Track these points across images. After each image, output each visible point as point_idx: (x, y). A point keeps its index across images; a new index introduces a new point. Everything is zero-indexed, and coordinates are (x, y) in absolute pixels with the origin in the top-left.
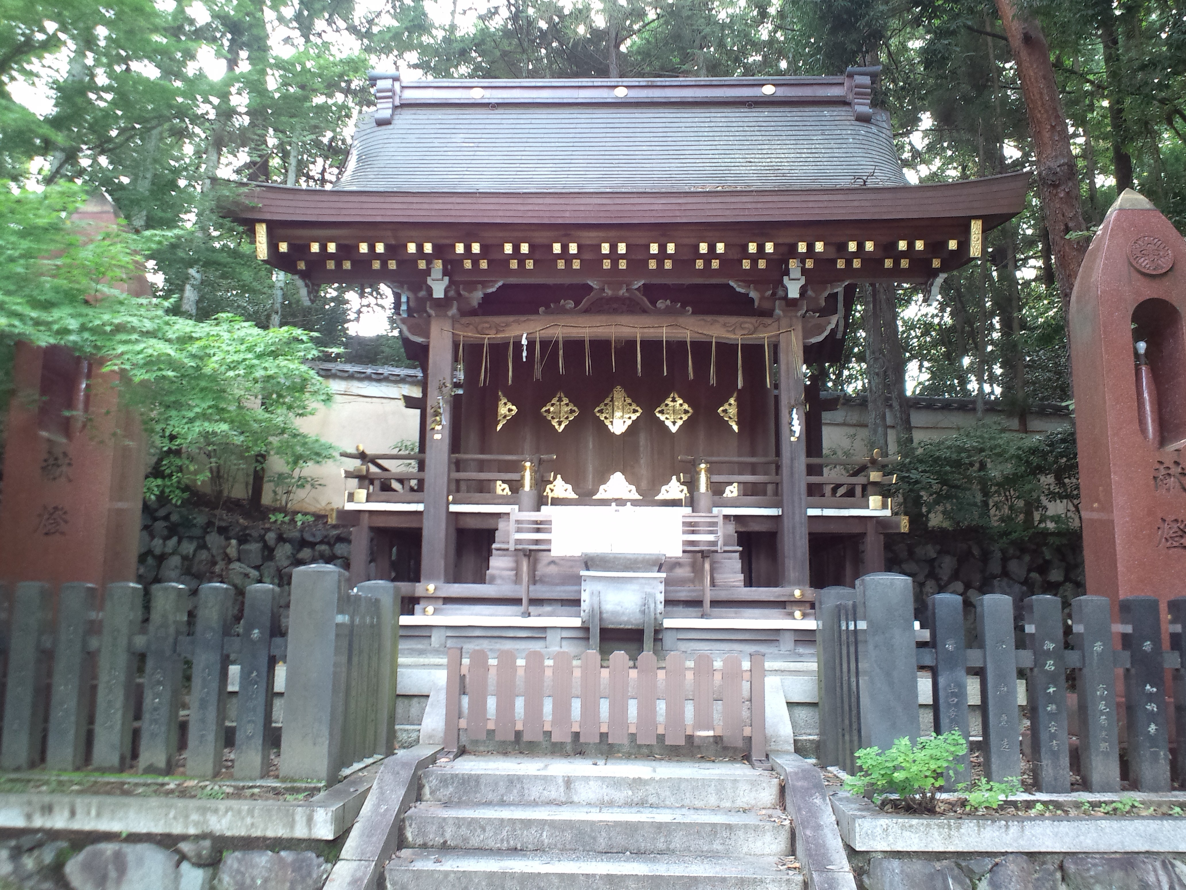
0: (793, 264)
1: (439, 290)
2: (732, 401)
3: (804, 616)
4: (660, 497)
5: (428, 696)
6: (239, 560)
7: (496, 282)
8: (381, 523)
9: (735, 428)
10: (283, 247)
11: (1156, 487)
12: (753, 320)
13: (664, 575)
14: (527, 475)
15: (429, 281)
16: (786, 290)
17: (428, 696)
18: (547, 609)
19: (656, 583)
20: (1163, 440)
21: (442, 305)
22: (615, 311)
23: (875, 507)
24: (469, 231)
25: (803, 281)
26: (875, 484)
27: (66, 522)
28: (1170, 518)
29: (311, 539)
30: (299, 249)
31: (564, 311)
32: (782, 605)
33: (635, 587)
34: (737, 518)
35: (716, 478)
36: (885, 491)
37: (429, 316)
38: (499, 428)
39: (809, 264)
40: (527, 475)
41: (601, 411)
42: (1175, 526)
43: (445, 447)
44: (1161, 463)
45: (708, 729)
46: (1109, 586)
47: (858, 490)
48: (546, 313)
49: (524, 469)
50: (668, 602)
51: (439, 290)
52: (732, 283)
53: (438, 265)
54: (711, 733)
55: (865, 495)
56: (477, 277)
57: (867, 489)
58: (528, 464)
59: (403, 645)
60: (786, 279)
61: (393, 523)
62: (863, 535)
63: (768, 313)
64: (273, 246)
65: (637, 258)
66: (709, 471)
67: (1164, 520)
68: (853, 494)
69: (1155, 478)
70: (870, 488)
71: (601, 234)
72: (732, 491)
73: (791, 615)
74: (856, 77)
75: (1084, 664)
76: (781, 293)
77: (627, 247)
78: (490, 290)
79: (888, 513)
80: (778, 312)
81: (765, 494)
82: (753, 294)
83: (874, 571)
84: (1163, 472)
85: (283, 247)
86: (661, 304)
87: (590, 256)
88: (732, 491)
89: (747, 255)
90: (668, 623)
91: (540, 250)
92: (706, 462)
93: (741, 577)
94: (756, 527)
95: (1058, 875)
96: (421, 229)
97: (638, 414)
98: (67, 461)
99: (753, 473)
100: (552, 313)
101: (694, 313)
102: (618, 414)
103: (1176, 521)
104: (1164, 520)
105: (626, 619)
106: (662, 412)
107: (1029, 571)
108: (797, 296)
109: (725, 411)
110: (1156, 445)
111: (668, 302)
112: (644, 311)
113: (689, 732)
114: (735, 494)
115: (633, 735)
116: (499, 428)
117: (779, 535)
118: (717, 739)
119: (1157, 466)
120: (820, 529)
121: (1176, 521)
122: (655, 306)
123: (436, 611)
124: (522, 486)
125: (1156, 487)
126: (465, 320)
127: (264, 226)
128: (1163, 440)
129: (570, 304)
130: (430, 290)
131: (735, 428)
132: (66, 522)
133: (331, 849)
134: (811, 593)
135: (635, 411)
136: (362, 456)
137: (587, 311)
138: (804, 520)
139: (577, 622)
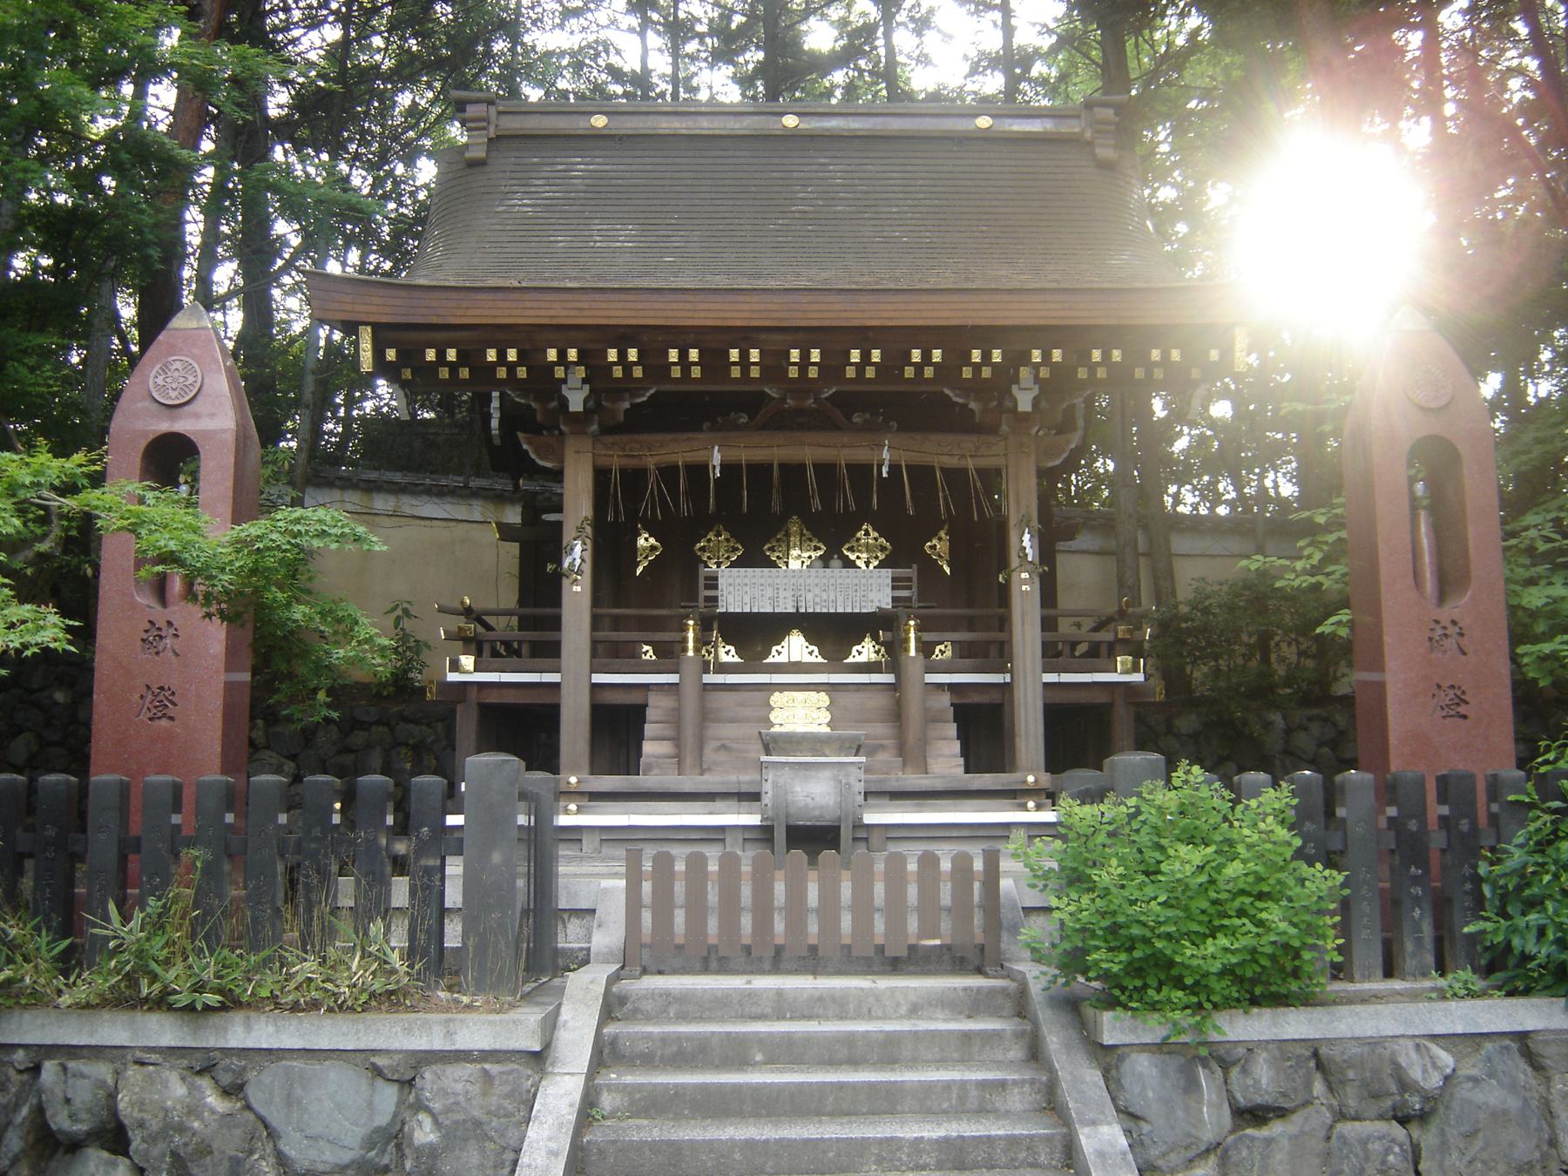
0: (1025, 373)
1: (576, 400)
2: (942, 534)
3: (1039, 807)
4: (850, 660)
5: (594, 911)
6: (268, 747)
7: (647, 389)
8: (493, 698)
9: (947, 570)
10: (391, 355)
11: (1432, 650)
12: (975, 438)
13: (863, 759)
14: (691, 635)
15: (565, 391)
16: (1015, 401)
17: (594, 911)
18: (719, 804)
19: (853, 770)
20: (1442, 597)
21: (579, 420)
22: (802, 427)
23: (1123, 672)
24: (623, 336)
25: (1036, 391)
26: (1123, 641)
27: (174, 704)
28: (1445, 684)
29: (366, 719)
30: (411, 355)
31: (737, 427)
32: (1016, 795)
33: (827, 773)
34: (952, 687)
35: (928, 637)
36: (1137, 651)
37: (561, 433)
38: (639, 570)
39: (1044, 373)
40: (691, 635)
41: (772, 549)
42: (1451, 693)
43: (586, 602)
44: (1437, 622)
45: (934, 938)
46: (1379, 761)
47: (1104, 650)
48: (711, 430)
49: (684, 629)
50: (867, 794)
51: (576, 400)
52: (947, 391)
53: (581, 372)
54: (938, 942)
55: (1112, 655)
56: (627, 386)
57: (1112, 650)
58: (691, 622)
59: (564, 851)
60: (1014, 388)
61: (510, 698)
62: (1110, 706)
63: (993, 430)
64: (378, 353)
65: (833, 366)
66: (919, 629)
67: (1439, 687)
68: (1099, 655)
69: (1430, 639)
70: (1118, 647)
71: (789, 337)
72: (943, 652)
73: (1024, 808)
74: (1096, 110)
75: (1346, 845)
76: (1008, 404)
77: (822, 354)
78: (639, 400)
79: (1138, 677)
80: (1004, 428)
81: (986, 656)
82: (973, 405)
83: (1122, 750)
84: (1440, 632)
85: (391, 355)
86: (856, 419)
87: (774, 365)
88: (943, 652)
89: (968, 363)
90: (870, 818)
91: (714, 361)
92: (916, 618)
93: (961, 761)
94: (976, 699)
95: (1312, 1064)
96: (562, 333)
97: (820, 553)
98: (172, 631)
99: (970, 630)
100: (720, 430)
101: (899, 430)
102: (795, 552)
103: (1452, 687)
104: (1439, 687)
105: (817, 813)
106: (851, 549)
107: (1319, 746)
108: (1029, 409)
109: (934, 547)
110: (1434, 601)
111: (867, 416)
112: (837, 427)
113: (912, 941)
114: (949, 653)
115: (849, 947)
116: (639, 570)
117: (1006, 708)
118: (947, 948)
119: (1433, 625)
120: (1059, 697)
121: (1452, 687)
122: (849, 419)
123: (579, 811)
124: (685, 650)
125: (1432, 650)
126: (610, 439)
127: (369, 329)
128: (1442, 597)
129: (744, 419)
130: (564, 403)
131: (947, 570)
132: (174, 704)
133: (539, 1059)
134: (1046, 780)
135: (816, 549)
136: (468, 612)
137: (763, 427)
138: (1040, 689)
139: (754, 820)
